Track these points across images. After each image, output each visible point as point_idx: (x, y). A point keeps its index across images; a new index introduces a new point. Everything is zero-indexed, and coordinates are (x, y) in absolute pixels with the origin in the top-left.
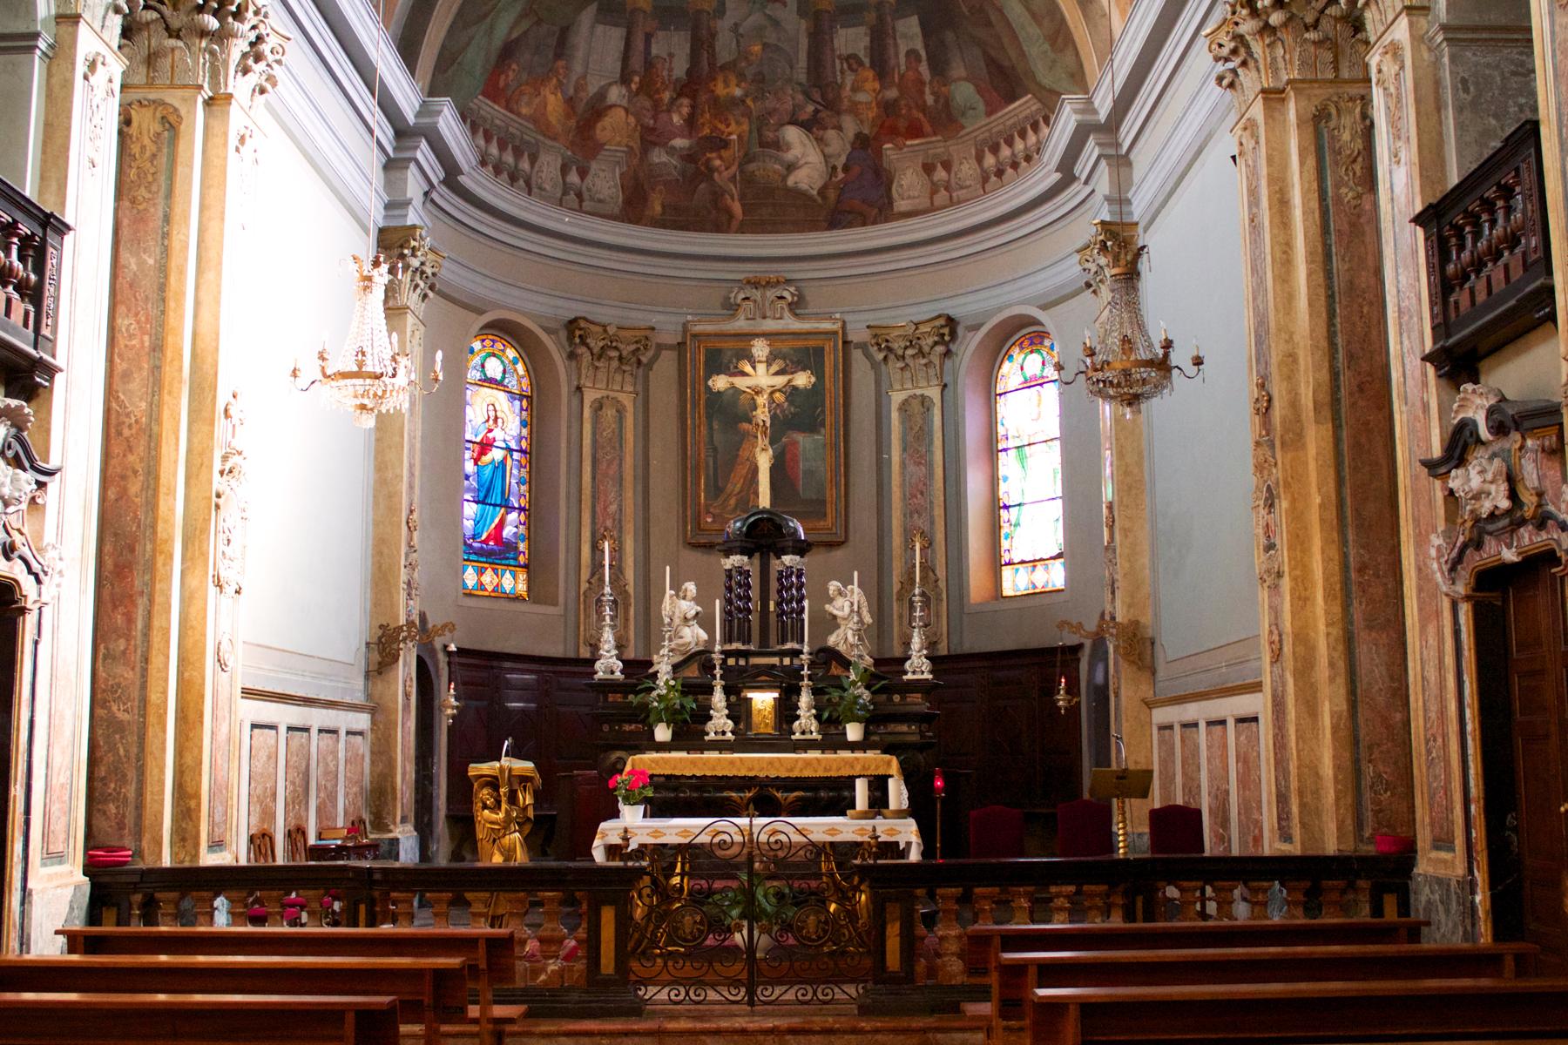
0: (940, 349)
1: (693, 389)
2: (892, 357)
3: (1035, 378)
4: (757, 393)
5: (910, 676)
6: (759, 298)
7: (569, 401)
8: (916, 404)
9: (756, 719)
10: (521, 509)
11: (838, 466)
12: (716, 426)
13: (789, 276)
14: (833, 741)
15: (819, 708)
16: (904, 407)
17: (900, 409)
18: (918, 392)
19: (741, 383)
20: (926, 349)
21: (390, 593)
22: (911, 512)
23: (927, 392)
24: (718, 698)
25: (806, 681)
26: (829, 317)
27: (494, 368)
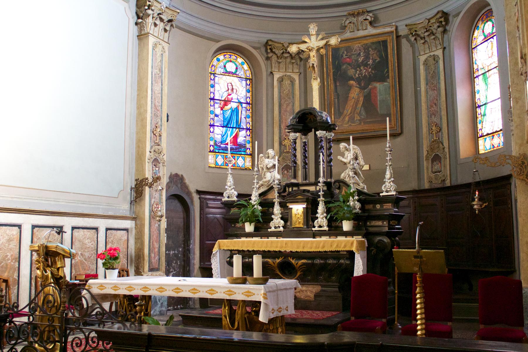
0: (441, 29)
1: (327, 68)
2: (418, 38)
3: (489, 34)
4: (310, 50)
5: (384, 194)
6: (355, 22)
7: (267, 79)
8: (431, 59)
9: (294, 219)
10: (247, 129)
11: (396, 96)
12: (338, 84)
13: (369, 9)
14: (334, 229)
15: (328, 211)
16: (426, 63)
17: (424, 64)
18: (432, 54)
19: (303, 47)
20: (434, 31)
21: (142, 164)
22: (431, 114)
23: (436, 53)
24: (277, 210)
25: (322, 198)
26: (389, 25)
27: (231, 67)
